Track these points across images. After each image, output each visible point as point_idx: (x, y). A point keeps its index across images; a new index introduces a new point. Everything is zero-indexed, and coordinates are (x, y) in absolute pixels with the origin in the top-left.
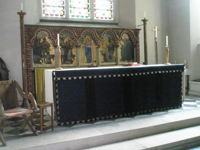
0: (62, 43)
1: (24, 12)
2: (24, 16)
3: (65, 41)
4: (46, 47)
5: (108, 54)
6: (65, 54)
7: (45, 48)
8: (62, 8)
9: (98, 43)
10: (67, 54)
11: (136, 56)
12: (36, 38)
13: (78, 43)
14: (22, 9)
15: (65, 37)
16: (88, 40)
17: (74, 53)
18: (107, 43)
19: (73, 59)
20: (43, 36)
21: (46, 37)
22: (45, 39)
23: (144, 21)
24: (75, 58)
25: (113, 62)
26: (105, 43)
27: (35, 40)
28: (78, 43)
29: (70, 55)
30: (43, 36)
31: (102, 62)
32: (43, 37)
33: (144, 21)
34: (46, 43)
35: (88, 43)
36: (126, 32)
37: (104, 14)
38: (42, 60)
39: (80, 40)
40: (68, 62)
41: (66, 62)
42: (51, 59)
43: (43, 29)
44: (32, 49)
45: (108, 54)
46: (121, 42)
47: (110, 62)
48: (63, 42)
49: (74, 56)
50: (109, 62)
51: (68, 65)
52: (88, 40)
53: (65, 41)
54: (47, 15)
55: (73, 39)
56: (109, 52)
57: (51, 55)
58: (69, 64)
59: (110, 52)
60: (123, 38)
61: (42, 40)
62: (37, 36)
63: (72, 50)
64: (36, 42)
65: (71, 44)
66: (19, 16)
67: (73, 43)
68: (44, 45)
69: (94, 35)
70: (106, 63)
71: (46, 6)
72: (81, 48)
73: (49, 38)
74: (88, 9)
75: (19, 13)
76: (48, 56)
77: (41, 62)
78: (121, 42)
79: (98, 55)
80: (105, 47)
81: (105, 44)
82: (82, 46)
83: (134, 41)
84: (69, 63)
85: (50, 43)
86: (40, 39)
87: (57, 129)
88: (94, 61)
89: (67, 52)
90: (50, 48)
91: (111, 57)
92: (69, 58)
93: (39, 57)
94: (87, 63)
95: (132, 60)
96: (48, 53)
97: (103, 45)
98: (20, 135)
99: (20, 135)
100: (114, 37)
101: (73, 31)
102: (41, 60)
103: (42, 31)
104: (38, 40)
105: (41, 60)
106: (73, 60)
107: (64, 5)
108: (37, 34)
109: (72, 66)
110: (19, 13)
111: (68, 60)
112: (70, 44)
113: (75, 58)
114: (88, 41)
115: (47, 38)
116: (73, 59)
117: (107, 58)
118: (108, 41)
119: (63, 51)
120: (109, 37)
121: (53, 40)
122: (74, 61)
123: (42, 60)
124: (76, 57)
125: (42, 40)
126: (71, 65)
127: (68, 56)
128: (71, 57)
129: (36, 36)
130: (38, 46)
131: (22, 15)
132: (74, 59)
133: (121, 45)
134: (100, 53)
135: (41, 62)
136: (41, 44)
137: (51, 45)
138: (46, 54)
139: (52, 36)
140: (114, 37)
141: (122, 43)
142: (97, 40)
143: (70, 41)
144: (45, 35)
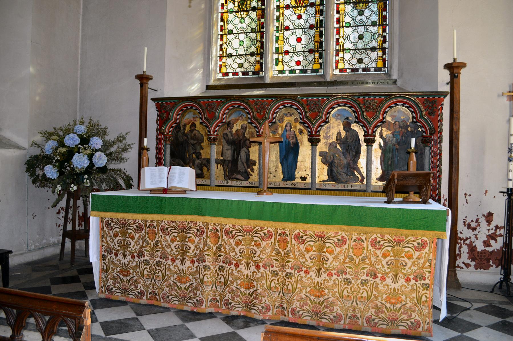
1: (149, 75)
2: (463, 71)
3: (234, 130)
4: (195, 142)
7: (193, 145)
8: (380, 54)
12: (175, 123)
14: (145, 70)
18: (339, 134)
19: (249, 170)
22: (194, 125)
23: (454, 69)
32: (191, 121)
33: (454, 69)
34: (195, 135)
36: (288, 103)
37: (360, 61)
41: (235, 176)
42: (204, 167)
44: (168, 146)
46: (384, 129)
48: (231, 132)
49: (254, 163)
51: (238, 183)
53: (234, 130)
54: (226, 74)
57: (204, 159)
58: (241, 180)
60: (388, 118)
62: (384, 118)
64: (177, 132)
66: (138, 82)
68: (192, 138)
71: (225, 56)
74: (318, 51)
75: (448, 66)
76: (197, 161)
79: (313, 162)
84: (241, 178)
85: (203, 134)
86: (185, 126)
89: (239, 154)
90: (202, 144)
92: (241, 167)
96: (199, 155)
104: (182, 128)
106: (251, 173)
107: (384, 45)
108: (385, 112)
109: (247, 185)
110: (448, 66)
111: (239, 173)
113: (254, 167)
115: (197, 123)
116: (249, 170)
118: (342, 128)
122: (251, 175)
124: (257, 164)
126: (245, 183)
127: (240, 162)
129: (381, 118)
130: (181, 139)
131: (143, 79)
132: (252, 170)
133: (381, 137)
134: (319, 159)
137: (205, 138)
138: (194, 156)
139: (306, 117)
140: (416, 118)
143: (246, 128)
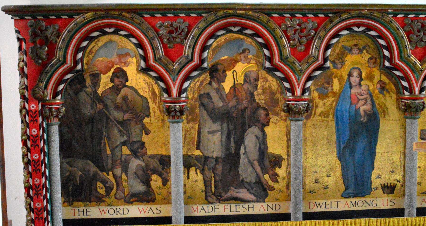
0: (208, 96)
3: (227, 85)
4: (126, 117)
6: (228, 149)
7: (122, 123)
9: (411, 90)
10: (238, 149)
13: (299, 92)
15: (233, 62)
16: (355, 73)
17: (275, 147)
19: (267, 177)
20: (115, 58)
21: (126, 64)
22: (120, 74)
24: (281, 172)
27: (72, 82)
28: (299, 92)
29: (254, 154)
30: (115, 58)
36: (358, 25)
38: (104, 182)
39: (309, 79)
40: (243, 194)
41: (233, 192)
42: (154, 177)
43: (235, 25)
48: (219, 90)
49: (277, 161)
52: (355, 73)
53: (227, 85)
55: (270, 71)
57: (153, 157)
58: (249, 202)
61: (105, 82)
63: (267, 129)
65: (260, 98)
67: (272, 93)
68: (117, 107)
69: (389, 48)
72: (316, 119)
73: (146, 70)
76: (135, 164)
77: (102, 191)
82: (319, 110)
86: (96, 77)
87: (173, 186)
89: (240, 142)
92: (246, 171)
93: (93, 168)
94: (345, 195)
101: (272, 32)
102: (99, 184)
103: (92, 39)
104: (88, 82)
105: (99, 184)
106: (271, 183)
111: (242, 184)
112: (257, 98)
113: (278, 170)
114: (355, 79)
115: (131, 70)
116: (267, 177)
119: (219, 134)
121: (160, 78)
122: (272, 189)
123: (104, 182)
124: (284, 164)
125: (105, 82)
127: (243, 160)
128: (258, 168)
132: (275, 177)
135: (102, 191)
136: (100, 99)
142: (407, 78)
143: (257, 79)
144: (124, 56)
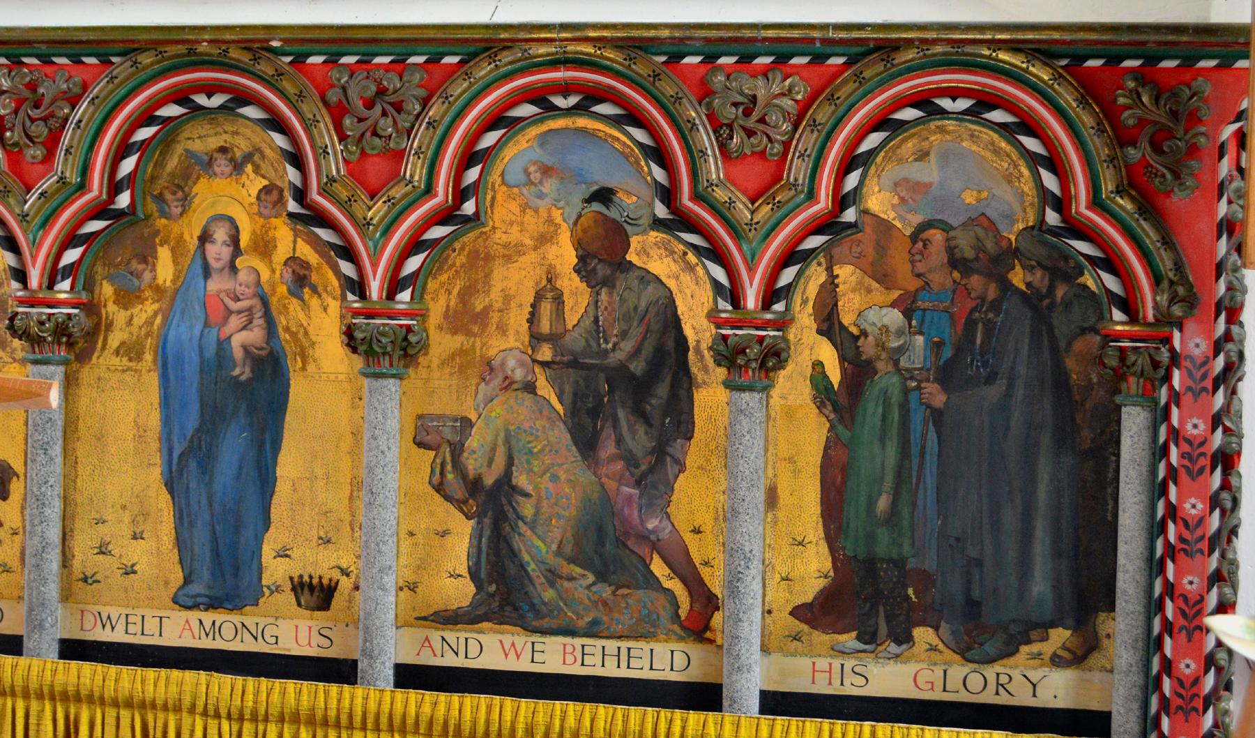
5: (557, 487)
11: (1155, 567)
16: (221, 234)
18: (548, 292)
25: (643, 631)
26: (514, 282)
31: (449, 618)
35: (215, 285)
45: (557, 487)
46: (846, 273)
47: (593, 631)
50: (569, 631)
52: (221, 234)
56: (587, 444)
59: (608, 449)
70: (522, 640)
78: (846, 273)
80: (519, 375)
81: (518, 320)
82: (115, 340)
83: (1112, 262)
88: (300, 587)
91: (614, 551)
94: (183, 601)
95: (1060, 636)
97: (482, 317)
98: (978, 341)
99: (978, 341)
100: (1061, 204)
103: (484, 157)
114: (218, 251)
117: (537, 547)
120: (604, 195)
133: (829, 325)
141: (869, 308)
